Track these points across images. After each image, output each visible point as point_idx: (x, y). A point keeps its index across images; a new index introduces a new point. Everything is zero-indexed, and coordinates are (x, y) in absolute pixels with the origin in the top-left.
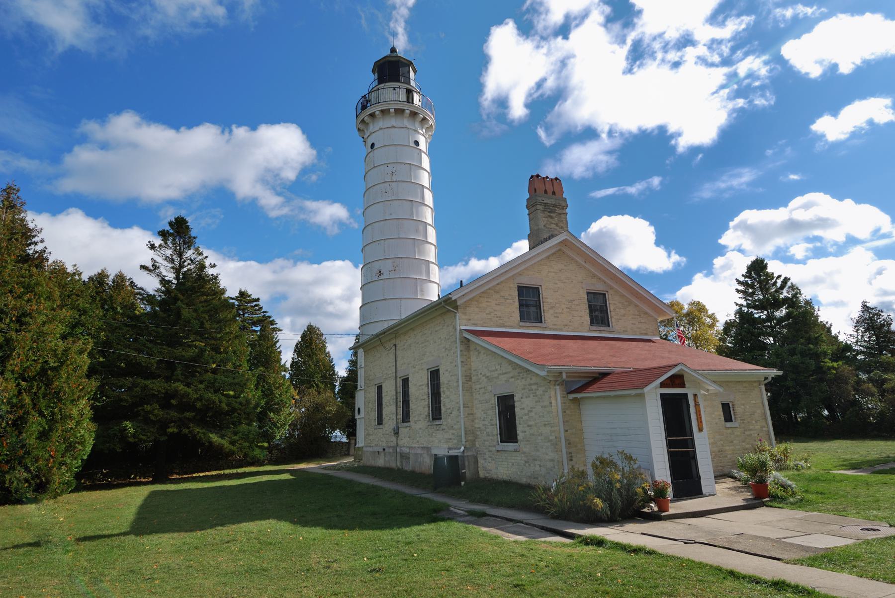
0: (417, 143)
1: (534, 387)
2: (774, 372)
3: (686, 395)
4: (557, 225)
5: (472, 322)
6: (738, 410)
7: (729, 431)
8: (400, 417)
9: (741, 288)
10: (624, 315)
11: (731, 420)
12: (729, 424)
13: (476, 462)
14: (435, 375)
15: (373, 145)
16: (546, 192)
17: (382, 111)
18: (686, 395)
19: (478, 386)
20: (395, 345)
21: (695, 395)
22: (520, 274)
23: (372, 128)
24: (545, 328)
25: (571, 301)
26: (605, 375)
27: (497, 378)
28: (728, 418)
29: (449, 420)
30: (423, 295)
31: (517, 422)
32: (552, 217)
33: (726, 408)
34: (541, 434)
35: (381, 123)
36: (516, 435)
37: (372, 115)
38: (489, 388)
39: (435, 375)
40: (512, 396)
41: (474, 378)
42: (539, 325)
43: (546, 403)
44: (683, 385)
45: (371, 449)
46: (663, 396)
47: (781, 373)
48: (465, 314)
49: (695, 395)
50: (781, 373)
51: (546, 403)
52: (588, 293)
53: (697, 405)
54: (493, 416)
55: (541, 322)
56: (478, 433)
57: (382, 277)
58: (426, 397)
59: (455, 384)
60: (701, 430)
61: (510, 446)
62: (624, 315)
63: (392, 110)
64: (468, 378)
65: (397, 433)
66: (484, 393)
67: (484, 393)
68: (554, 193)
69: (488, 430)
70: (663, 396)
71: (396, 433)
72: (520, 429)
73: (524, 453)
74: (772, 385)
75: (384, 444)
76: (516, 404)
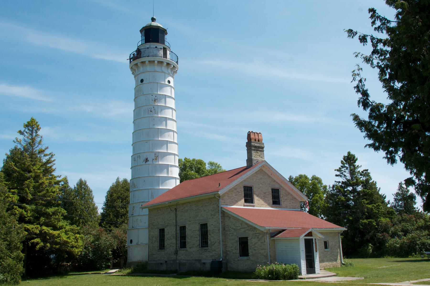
0: (169, 82)
1: (257, 235)
2: (345, 229)
3: (312, 239)
4: (259, 156)
5: (226, 203)
6: (330, 244)
7: (326, 252)
8: (179, 245)
9: (365, 115)
10: (286, 200)
11: (327, 248)
12: (326, 250)
13: (227, 265)
14: (204, 227)
15: (142, 81)
16: (255, 140)
17: (149, 61)
18: (312, 239)
19: (229, 233)
20: (176, 209)
21: (315, 239)
22: (245, 181)
23: (141, 69)
24: (254, 206)
25: (265, 193)
26: (284, 230)
27: (240, 230)
28: (326, 247)
29: (213, 247)
30: (172, 174)
31: (249, 248)
32: (257, 153)
33: (326, 243)
34: (260, 253)
35: (149, 68)
36: (248, 253)
37: (143, 63)
38: (235, 234)
39: (204, 227)
40: (247, 238)
41: (226, 229)
42: (252, 204)
43: (263, 241)
44: (311, 236)
45: (155, 262)
46: (305, 239)
47: (346, 229)
48: (223, 200)
49: (315, 239)
50: (346, 229)
51: (263, 241)
52: (272, 189)
53: (316, 243)
54: (237, 245)
55: (252, 203)
56: (228, 253)
57: (148, 163)
58: (198, 236)
59: (217, 231)
60: (316, 251)
61: (245, 258)
62: (286, 200)
63: (156, 62)
64: (224, 229)
65: (177, 253)
66: (232, 236)
67: (232, 236)
68: (259, 141)
69: (233, 252)
70: (305, 239)
71: (176, 253)
72: (250, 251)
73: (252, 260)
74: (344, 234)
75: (166, 259)
76: (249, 241)
